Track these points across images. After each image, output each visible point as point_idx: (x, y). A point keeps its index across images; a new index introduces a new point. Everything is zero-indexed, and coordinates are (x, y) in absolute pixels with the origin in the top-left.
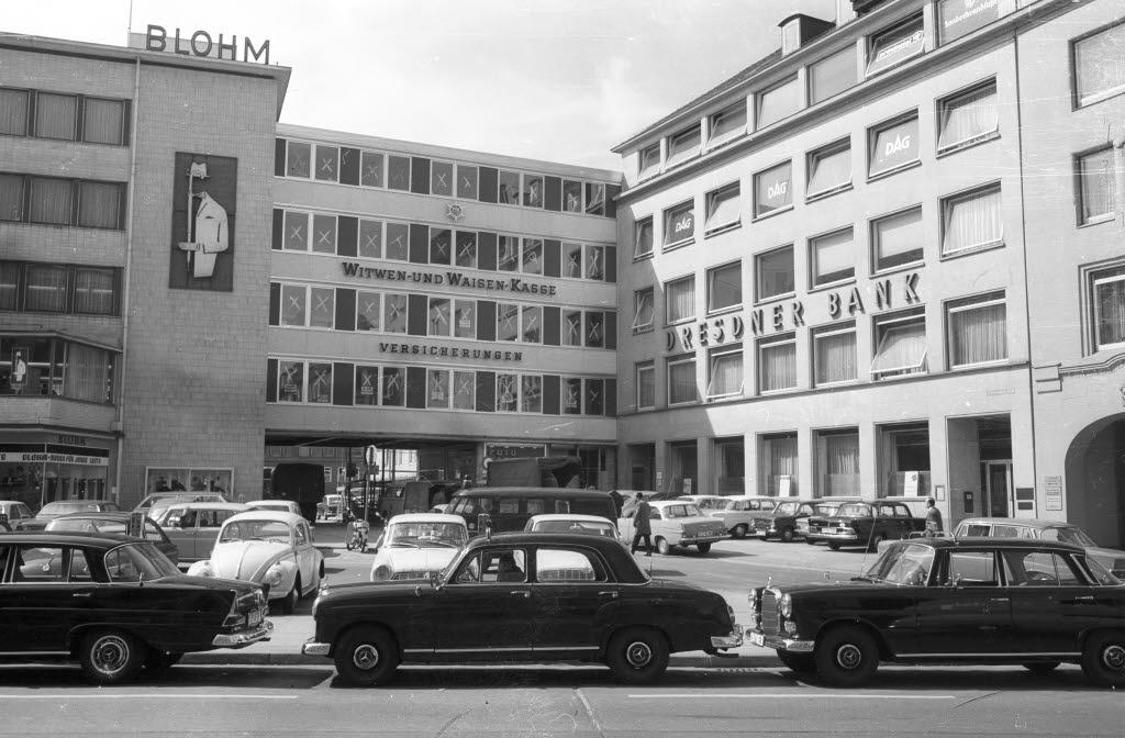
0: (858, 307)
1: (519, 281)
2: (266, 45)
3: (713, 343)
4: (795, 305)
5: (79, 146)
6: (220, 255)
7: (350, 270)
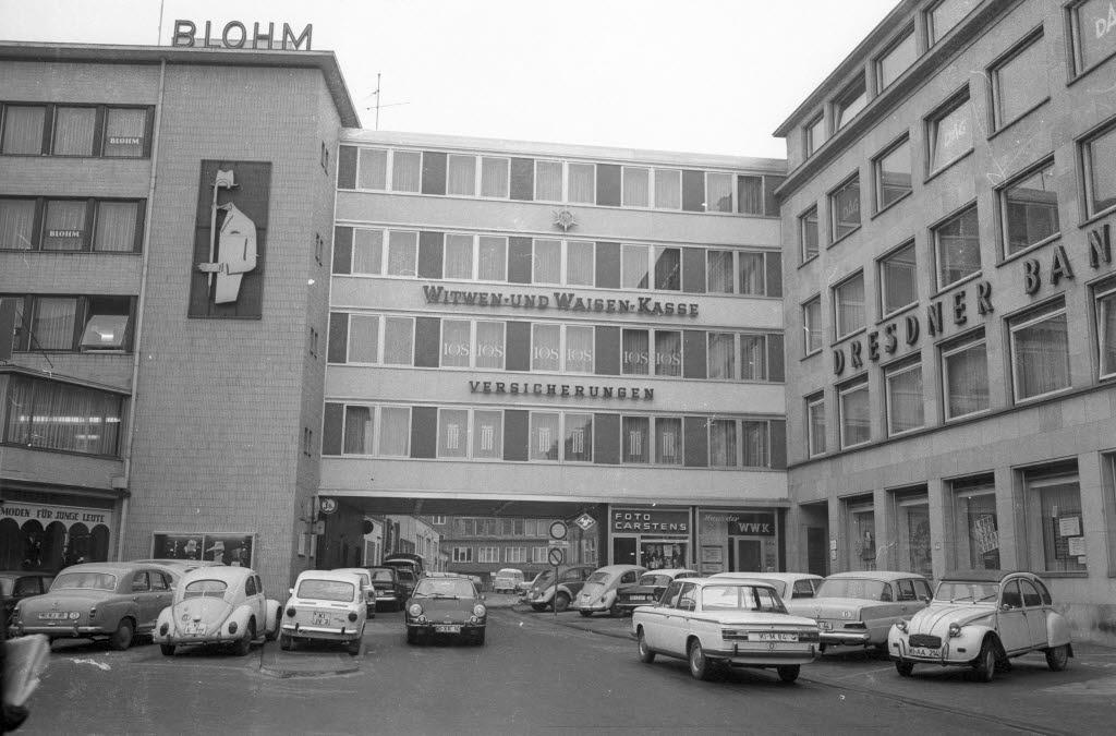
0: (1066, 272)
1: (648, 300)
2: (308, 32)
3: (885, 358)
4: (981, 287)
5: (96, 162)
6: (246, 275)
7: (433, 296)
